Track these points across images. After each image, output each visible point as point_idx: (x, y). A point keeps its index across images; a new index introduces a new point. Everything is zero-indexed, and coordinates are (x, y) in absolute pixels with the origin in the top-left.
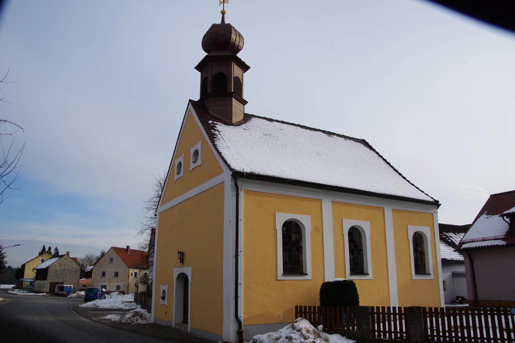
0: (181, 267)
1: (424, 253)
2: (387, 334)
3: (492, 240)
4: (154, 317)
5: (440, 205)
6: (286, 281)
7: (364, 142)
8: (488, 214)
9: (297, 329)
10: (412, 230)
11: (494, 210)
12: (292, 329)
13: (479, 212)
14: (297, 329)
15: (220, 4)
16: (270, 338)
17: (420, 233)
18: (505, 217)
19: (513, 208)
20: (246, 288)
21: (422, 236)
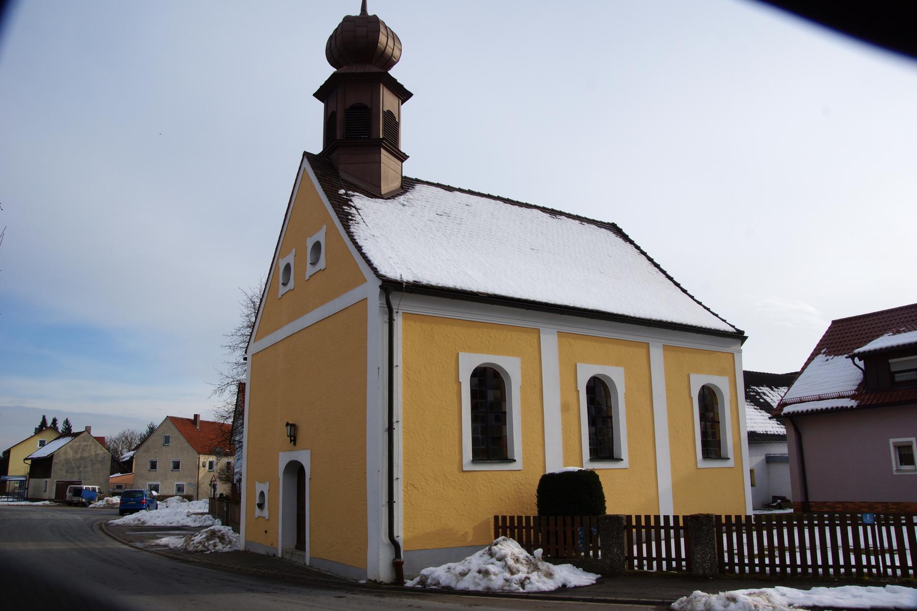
1: (719, 422)
2: (655, 563)
7: (614, 228)
8: (828, 354)
10: (697, 382)
18: (856, 359)
20: (408, 485)
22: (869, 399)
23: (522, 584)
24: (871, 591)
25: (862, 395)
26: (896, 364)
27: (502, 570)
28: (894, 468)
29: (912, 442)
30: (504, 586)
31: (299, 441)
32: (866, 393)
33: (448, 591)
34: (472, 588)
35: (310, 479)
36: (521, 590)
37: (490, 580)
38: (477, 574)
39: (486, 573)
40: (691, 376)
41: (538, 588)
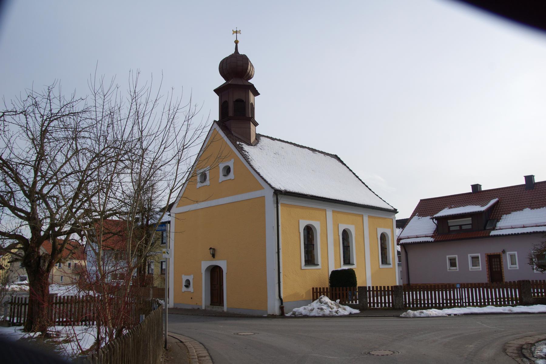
0: (212, 260)
1: (386, 249)
2: (379, 304)
3: (423, 237)
4: (173, 303)
5: (398, 212)
6: (306, 270)
7: (336, 157)
8: (419, 215)
9: (324, 303)
10: (380, 231)
11: (423, 212)
12: (320, 303)
13: (412, 214)
14: (324, 303)
15: (233, 34)
16: (306, 310)
17: (384, 234)
18: (434, 220)
19: (439, 213)
20: (284, 275)
21: (385, 236)
22: (439, 238)
23: (336, 312)
24: (462, 309)
25: (435, 235)
26: (451, 222)
27: (327, 308)
28: (448, 269)
29: (456, 257)
30: (330, 314)
31: (216, 256)
32: (437, 235)
33: (306, 316)
34: (317, 315)
35: (226, 273)
36: (337, 315)
37: (324, 311)
38: (318, 310)
39: (322, 309)
40: (378, 228)
41: (343, 314)
